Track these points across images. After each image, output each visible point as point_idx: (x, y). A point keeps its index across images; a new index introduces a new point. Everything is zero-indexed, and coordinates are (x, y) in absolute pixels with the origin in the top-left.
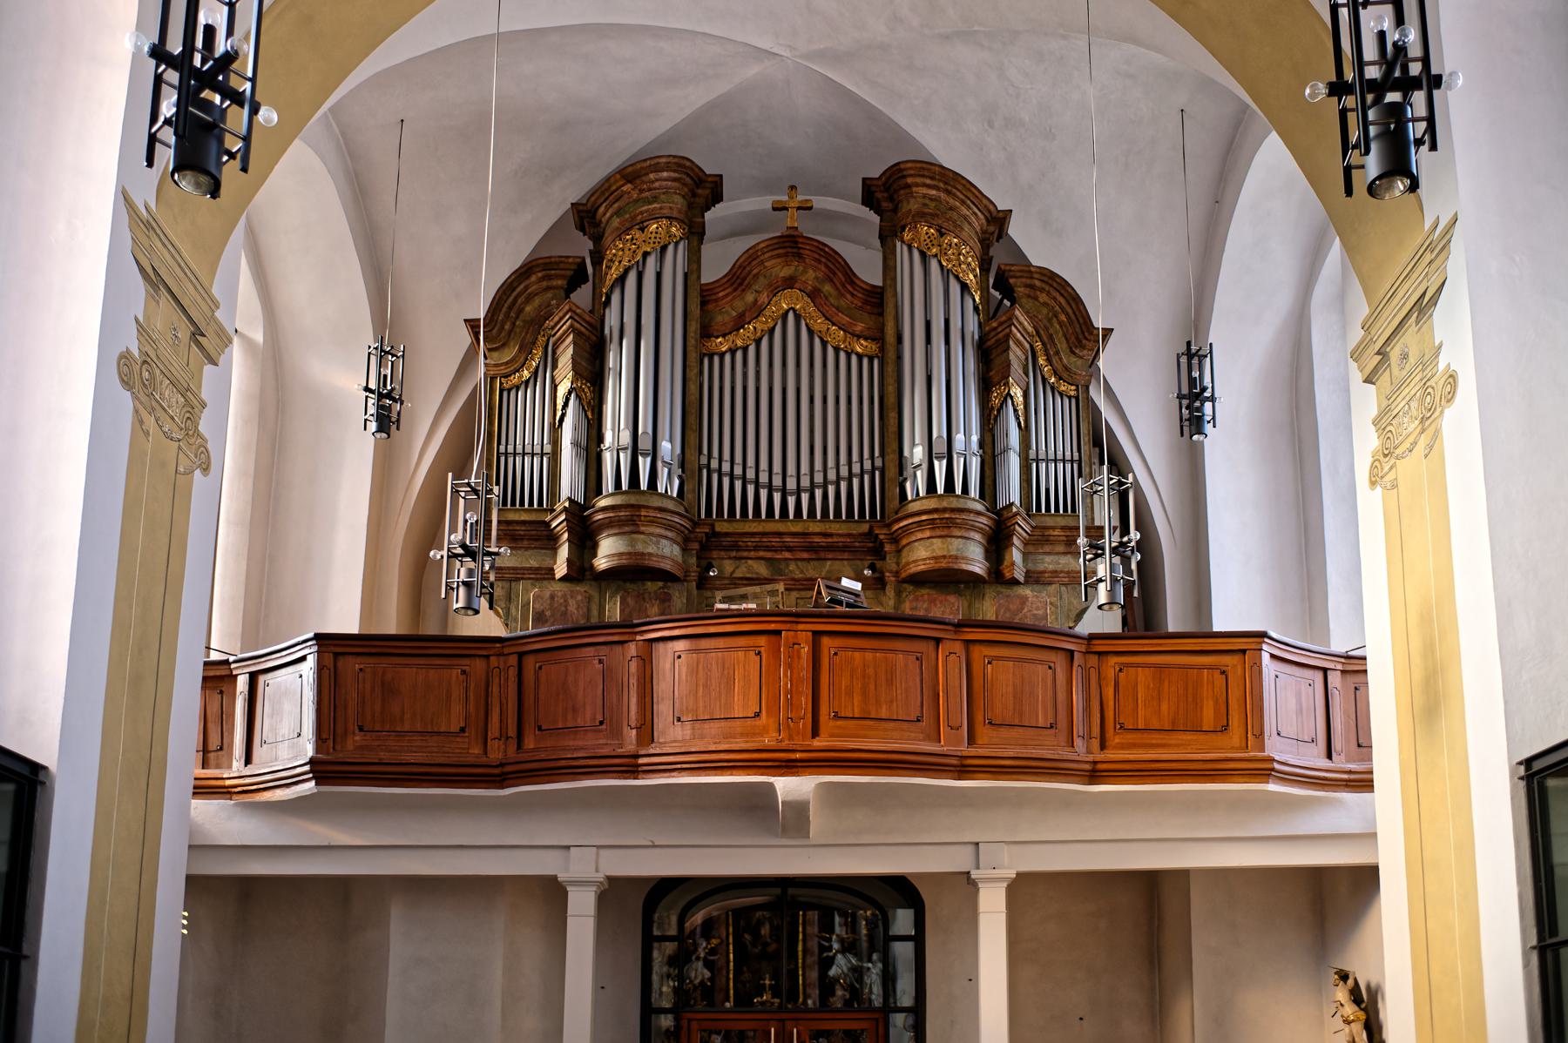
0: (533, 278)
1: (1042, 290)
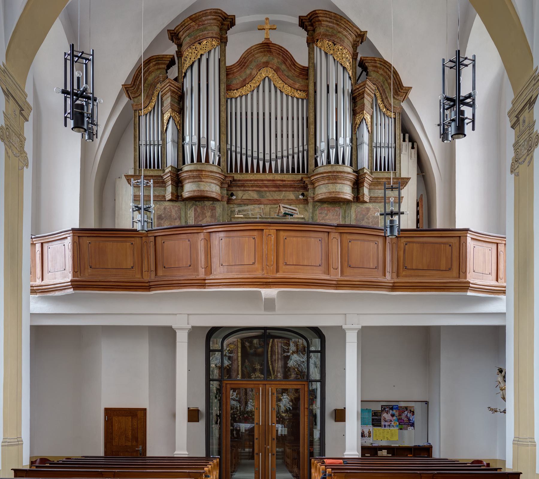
0: (151, 64)
1: (380, 68)
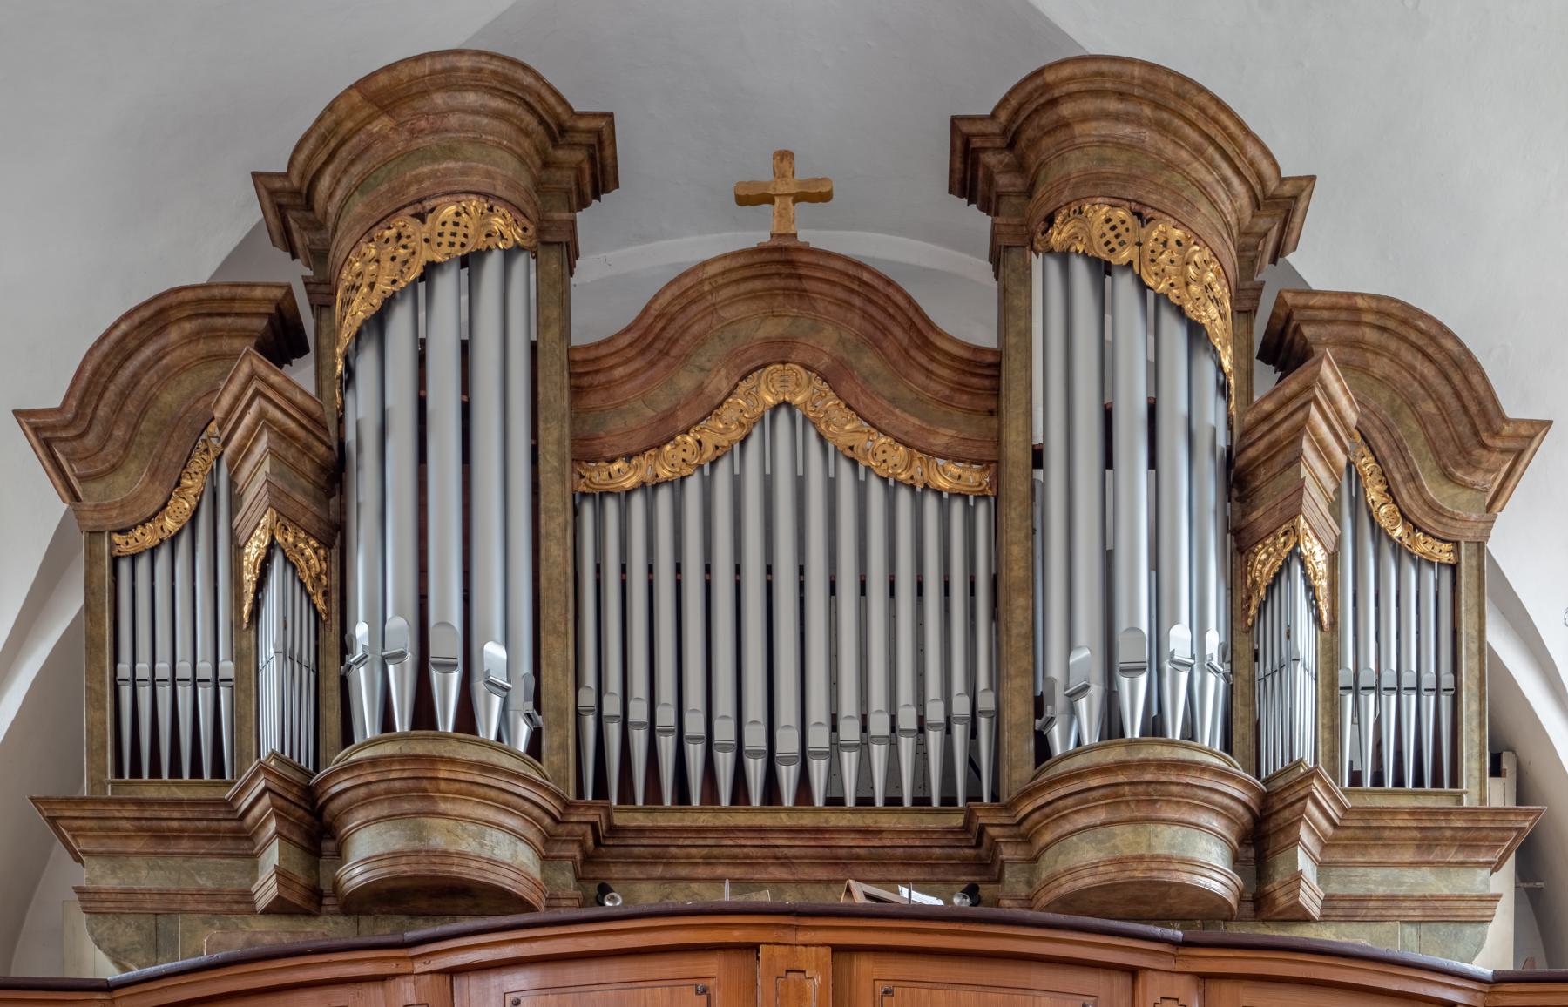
0: (174, 334)
1: (1379, 350)
